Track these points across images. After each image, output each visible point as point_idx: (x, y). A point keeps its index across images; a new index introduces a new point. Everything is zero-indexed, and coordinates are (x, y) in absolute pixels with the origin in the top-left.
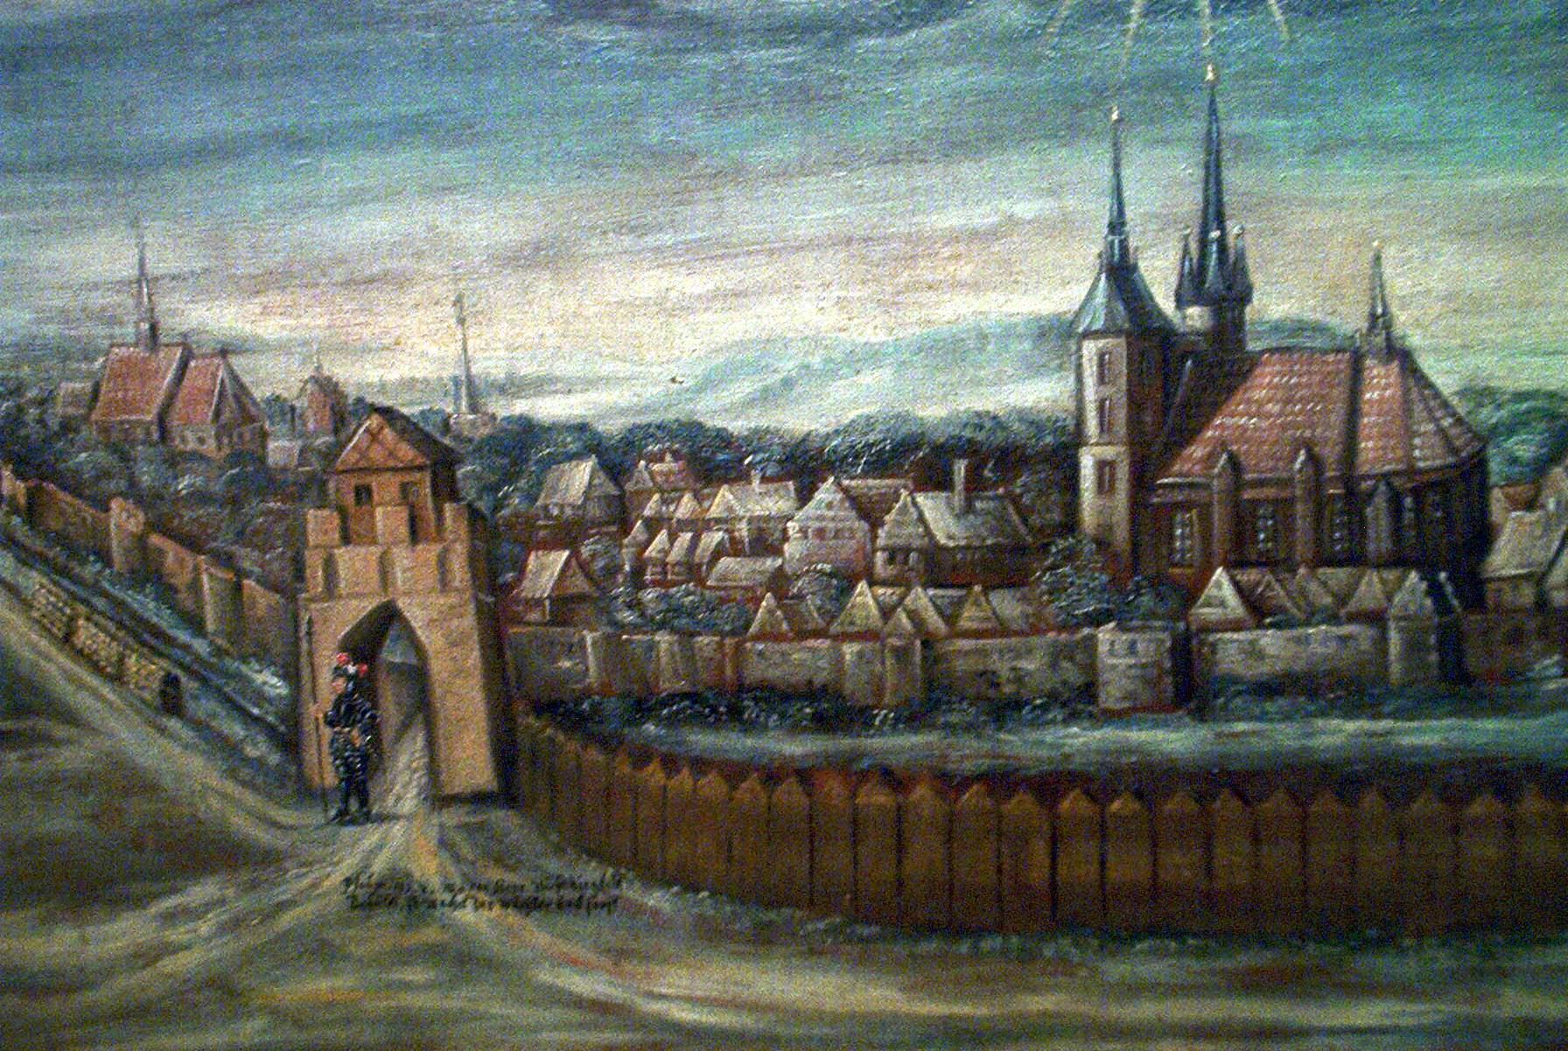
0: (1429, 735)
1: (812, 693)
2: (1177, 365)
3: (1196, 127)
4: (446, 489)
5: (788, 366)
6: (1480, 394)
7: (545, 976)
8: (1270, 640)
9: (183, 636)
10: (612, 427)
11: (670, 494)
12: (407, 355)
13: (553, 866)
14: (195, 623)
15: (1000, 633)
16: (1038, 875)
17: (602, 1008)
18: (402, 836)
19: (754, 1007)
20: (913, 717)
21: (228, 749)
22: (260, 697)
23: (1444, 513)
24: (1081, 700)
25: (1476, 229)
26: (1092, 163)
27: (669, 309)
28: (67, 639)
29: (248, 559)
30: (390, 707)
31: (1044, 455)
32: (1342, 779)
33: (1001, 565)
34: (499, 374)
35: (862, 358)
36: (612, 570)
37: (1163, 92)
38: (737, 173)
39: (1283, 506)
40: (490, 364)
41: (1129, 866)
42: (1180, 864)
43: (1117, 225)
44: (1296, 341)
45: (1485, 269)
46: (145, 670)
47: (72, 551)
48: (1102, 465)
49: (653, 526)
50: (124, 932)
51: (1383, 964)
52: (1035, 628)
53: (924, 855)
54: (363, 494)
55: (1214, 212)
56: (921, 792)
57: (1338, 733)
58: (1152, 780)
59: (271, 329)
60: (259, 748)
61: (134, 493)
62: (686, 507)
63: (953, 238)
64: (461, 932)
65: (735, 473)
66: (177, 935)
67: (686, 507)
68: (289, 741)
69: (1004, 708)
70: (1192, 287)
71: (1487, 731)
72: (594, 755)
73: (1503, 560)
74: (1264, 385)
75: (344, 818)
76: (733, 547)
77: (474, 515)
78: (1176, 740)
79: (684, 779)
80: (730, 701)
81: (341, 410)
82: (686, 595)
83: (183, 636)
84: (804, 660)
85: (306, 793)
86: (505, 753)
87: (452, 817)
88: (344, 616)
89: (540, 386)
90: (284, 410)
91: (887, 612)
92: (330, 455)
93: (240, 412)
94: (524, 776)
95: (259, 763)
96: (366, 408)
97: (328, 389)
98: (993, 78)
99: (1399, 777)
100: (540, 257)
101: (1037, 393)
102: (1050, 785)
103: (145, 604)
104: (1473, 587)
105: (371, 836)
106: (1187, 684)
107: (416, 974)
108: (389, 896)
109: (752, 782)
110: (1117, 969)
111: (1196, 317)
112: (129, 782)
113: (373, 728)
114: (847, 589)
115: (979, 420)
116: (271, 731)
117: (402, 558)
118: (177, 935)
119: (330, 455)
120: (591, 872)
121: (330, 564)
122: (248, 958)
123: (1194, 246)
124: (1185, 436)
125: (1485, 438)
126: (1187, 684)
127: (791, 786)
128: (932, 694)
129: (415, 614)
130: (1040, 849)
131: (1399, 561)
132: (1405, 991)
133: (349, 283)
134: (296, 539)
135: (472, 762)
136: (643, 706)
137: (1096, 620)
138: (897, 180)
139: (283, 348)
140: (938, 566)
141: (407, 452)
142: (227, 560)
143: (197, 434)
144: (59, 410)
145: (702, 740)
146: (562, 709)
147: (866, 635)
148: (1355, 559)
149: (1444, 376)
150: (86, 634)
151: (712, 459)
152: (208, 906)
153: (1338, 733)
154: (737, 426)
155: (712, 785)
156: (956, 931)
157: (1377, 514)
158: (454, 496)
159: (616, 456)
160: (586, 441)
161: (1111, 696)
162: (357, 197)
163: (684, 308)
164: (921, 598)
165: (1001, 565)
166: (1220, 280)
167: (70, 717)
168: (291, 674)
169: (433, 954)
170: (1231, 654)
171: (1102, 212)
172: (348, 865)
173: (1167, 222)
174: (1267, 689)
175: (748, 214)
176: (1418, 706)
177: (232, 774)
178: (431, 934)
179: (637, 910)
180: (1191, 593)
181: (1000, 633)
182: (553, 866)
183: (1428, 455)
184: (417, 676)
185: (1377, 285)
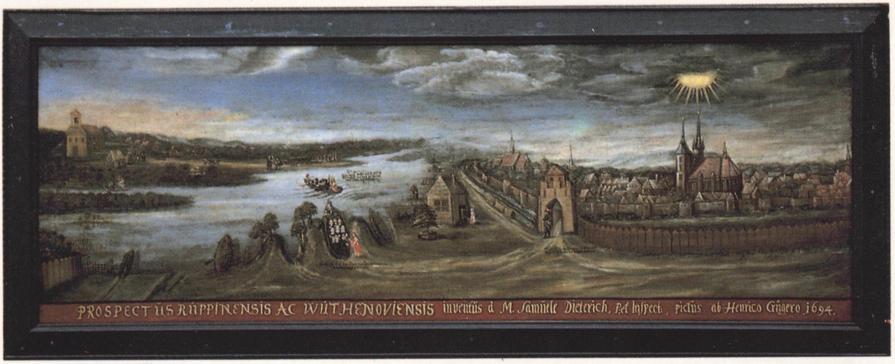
0: (733, 219)
1: (631, 214)
2: (692, 158)
3: (696, 120)
4: (567, 178)
5: (628, 158)
6: (741, 164)
7: (582, 264)
8: (707, 204)
9: (516, 205)
10: (597, 168)
11: (607, 180)
12: (560, 155)
13: (585, 245)
14: (519, 203)
15: (663, 203)
16: (669, 245)
17: (591, 270)
18: (557, 240)
19: (618, 269)
20: (647, 218)
21: (523, 225)
22: (530, 215)
23: (735, 183)
24: (676, 214)
25: (740, 138)
26: (677, 127)
27: (607, 148)
28: (493, 206)
29: (529, 191)
30: (555, 216)
31: (669, 174)
32: (720, 227)
33: (663, 191)
34: (577, 158)
35: (640, 157)
36: (596, 193)
37: (691, 115)
38: (620, 127)
39: (709, 183)
40: (576, 156)
41: (685, 243)
42: (693, 242)
43: (683, 137)
44: (711, 155)
45: (741, 144)
46: (509, 211)
47: (496, 189)
48: (680, 176)
49: (604, 185)
50: (502, 259)
51: (725, 258)
52: (668, 202)
53: (650, 242)
54: (552, 179)
55: (699, 134)
56: (649, 230)
57: (719, 219)
58: (688, 228)
59: (536, 150)
60: (530, 225)
61: (508, 179)
62: (609, 182)
63: (656, 137)
64: (566, 257)
65: (618, 176)
66: (511, 259)
67: (609, 182)
68: (535, 222)
69: (664, 216)
70: (695, 146)
71: (742, 219)
72: (592, 224)
73: (745, 190)
74: (707, 161)
75: (545, 237)
76: (617, 188)
77: (572, 183)
78: (693, 221)
79: (608, 229)
80: (618, 216)
81: (549, 165)
82: (609, 197)
83: (516, 205)
84: (630, 208)
85: (538, 233)
86: (576, 225)
87: (566, 236)
88: (545, 202)
89: (585, 161)
90: (537, 164)
91: (644, 200)
92: (546, 172)
93: (529, 164)
94: (579, 228)
95: (530, 228)
96: (552, 164)
97: (546, 161)
98: (665, 112)
99: (729, 226)
100: (586, 139)
101: (668, 163)
102: (671, 229)
103: (510, 199)
104: (740, 195)
105: (550, 240)
106: (694, 212)
107: (558, 265)
108: (555, 251)
109: (620, 229)
110: (682, 260)
111: (696, 151)
112: (502, 231)
113: (552, 221)
114: (637, 196)
115: (660, 167)
116: (532, 222)
117: (558, 190)
118: (511, 259)
119: (546, 172)
120: (590, 245)
121: (545, 192)
122: (525, 264)
123: (775, 275)
124: (694, 170)
125: (742, 171)
126: (694, 212)
127: (627, 230)
128: (652, 214)
129: (559, 200)
130: (669, 240)
131: (728, 191)
132: (730, 262)
133: (551, 143)
134: (539, 188)
135: (569, 227)
136: (601, 216)
137: (679, 201)
138: (647, 128)
139: (537, 153)
140: (652, 192)
141: (560, 172)
142: (525, 191)
143: (520, 167)
144: (495, 163)
145: (611, 222)
146: (587, 217)
147: (640, 204)
148: (721, 191)
149: (735, 161)
150: (497, 204)
151: (614, 173)
152: (518, 254)
153: (719, 219)
154: (619, 168)
155: (613, 229)
156: (654, 255)
157: (724, 183)
158: (568, 179)
159: (598, 173)
160: (592, 170)
161: (681, 214)
162: (553, 128)
163: (611, 148)
164: (650, 197)
165: (663, 191)
166: (699, 145)
167: (493, 220)
168: (537, 212)
169: (560, 261)
170: (701, 206)
171: (680, 134)
172: (545, 245)
173: (692, 136)
174: (707, 212)
175: (622, 132)
176: (732, 215)
177: (524, 229)
178: (560, 258)
179: (599, 252)
180: (694, 197)
181: (663, 203)
182: (585, 245)
183: (732, 174)
184: (560, 212)
185: (725, 148)
